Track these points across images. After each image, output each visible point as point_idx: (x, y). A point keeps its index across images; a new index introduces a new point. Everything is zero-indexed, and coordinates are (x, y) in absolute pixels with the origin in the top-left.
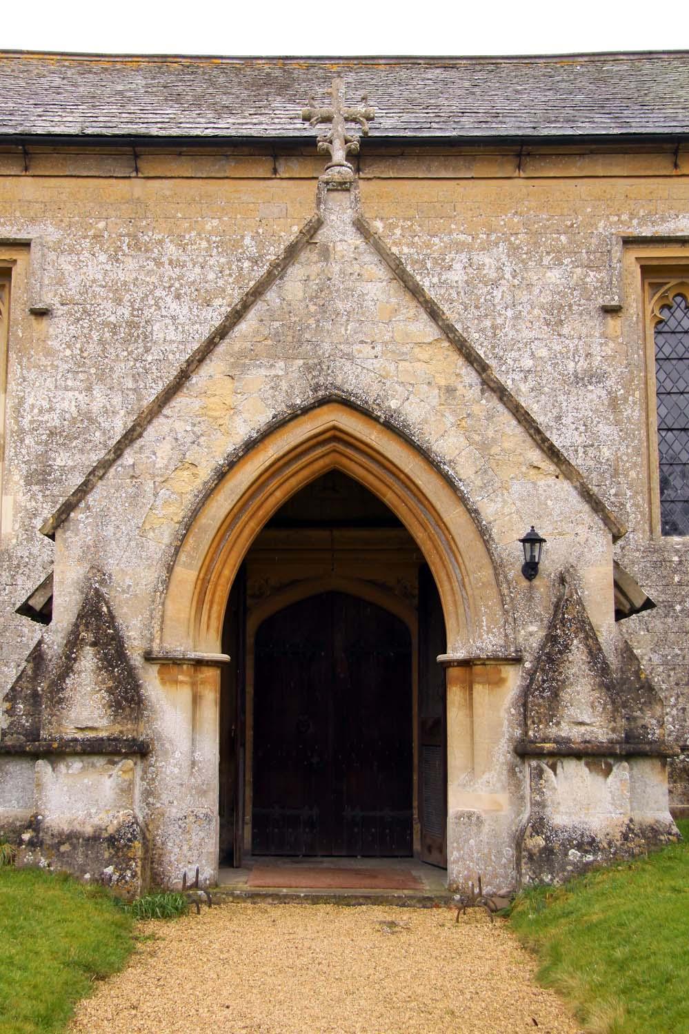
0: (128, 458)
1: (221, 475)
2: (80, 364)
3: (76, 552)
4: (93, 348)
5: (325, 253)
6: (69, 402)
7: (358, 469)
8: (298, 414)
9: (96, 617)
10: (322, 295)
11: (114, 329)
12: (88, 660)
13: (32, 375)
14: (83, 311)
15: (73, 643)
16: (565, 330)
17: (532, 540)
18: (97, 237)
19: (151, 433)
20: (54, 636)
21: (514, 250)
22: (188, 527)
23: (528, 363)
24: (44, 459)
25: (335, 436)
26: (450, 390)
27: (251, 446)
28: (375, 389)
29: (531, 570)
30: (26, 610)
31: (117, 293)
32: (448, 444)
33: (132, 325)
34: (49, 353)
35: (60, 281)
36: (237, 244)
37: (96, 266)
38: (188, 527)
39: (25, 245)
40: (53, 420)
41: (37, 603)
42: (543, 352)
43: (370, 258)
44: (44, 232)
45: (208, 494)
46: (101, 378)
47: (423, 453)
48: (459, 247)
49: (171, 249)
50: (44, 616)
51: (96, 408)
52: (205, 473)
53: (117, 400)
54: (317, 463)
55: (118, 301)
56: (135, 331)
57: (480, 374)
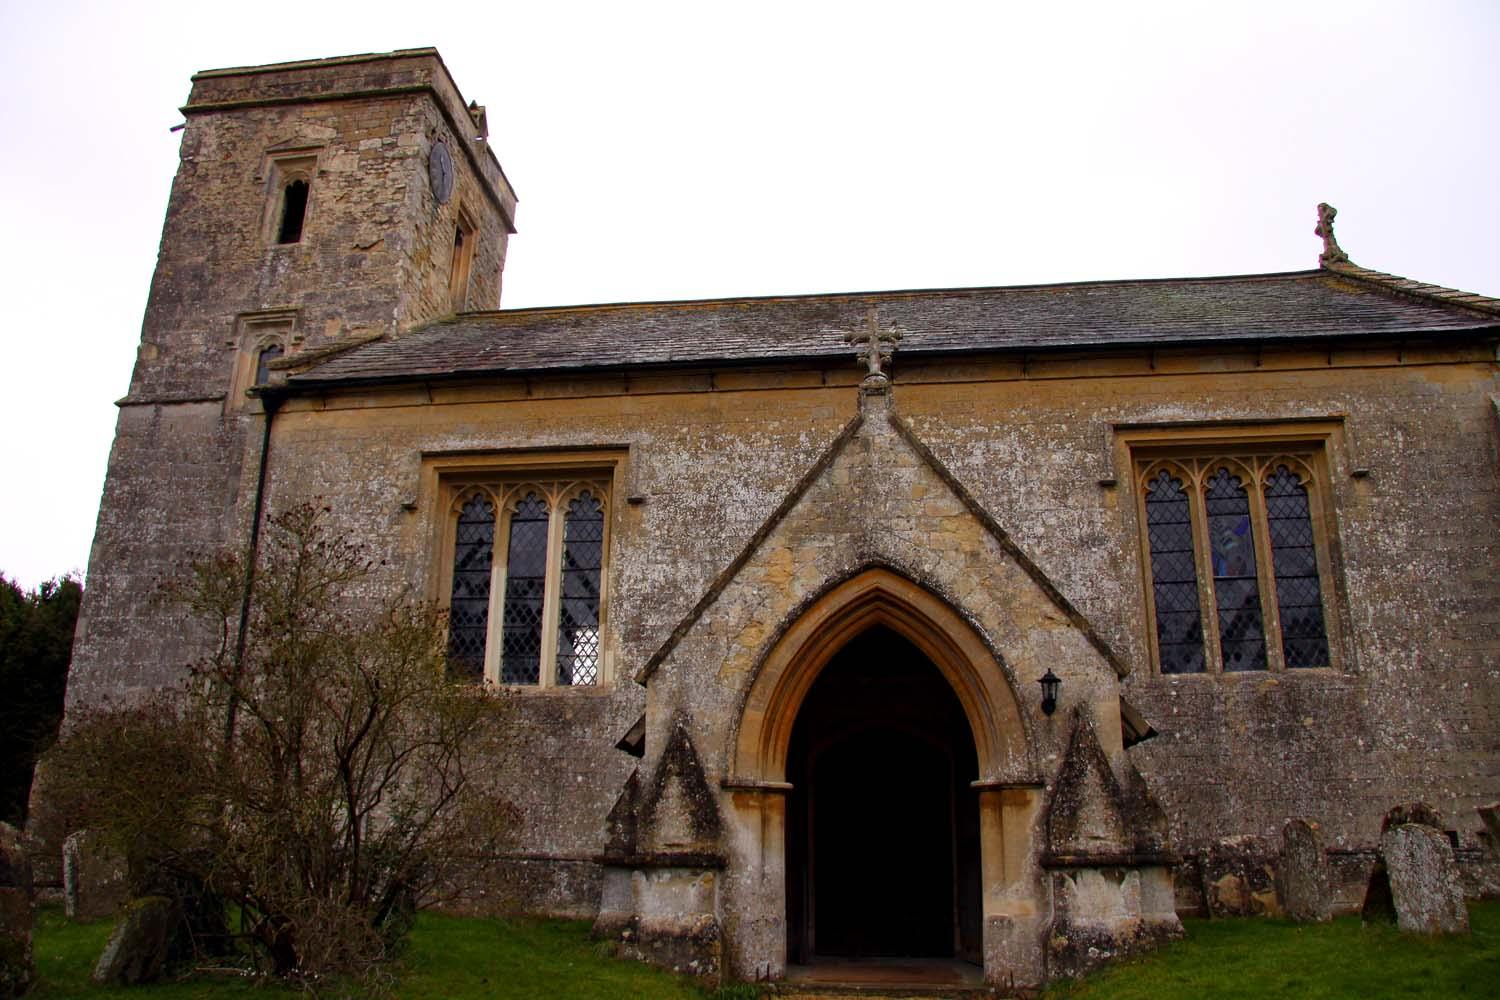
3: (664, 696)
4: (678, 529)
5: (866, 445)
6: (658, 574)
9: (681, 752)
11: (695, 512)
12: (674, 788)
13: (629, 551)
15: (662, 773)
16: (1071, 502)
17: (1050, 680)
19: (724, 597)
21: (1023, 438)
23: (1040, 530)
24: (638, 620)
26: (974, 555)
27: (807, 606)
29: (1049, 706)
30: (623, 745)
31: (697, 483)
32: (974, 600)
33: (709, 508)
34: (643, 533)
35: (652, 475)
36: (794, 440)
37: (680, 462)
42: (1053, 521)
46: (684, 552)
48: (979, 436)
49: (741, 447)
51: (680, 577)
52: (770, 628)
53: (697, 570)
54: (866, 617)
55: (698, 490)
56: (712, 515)
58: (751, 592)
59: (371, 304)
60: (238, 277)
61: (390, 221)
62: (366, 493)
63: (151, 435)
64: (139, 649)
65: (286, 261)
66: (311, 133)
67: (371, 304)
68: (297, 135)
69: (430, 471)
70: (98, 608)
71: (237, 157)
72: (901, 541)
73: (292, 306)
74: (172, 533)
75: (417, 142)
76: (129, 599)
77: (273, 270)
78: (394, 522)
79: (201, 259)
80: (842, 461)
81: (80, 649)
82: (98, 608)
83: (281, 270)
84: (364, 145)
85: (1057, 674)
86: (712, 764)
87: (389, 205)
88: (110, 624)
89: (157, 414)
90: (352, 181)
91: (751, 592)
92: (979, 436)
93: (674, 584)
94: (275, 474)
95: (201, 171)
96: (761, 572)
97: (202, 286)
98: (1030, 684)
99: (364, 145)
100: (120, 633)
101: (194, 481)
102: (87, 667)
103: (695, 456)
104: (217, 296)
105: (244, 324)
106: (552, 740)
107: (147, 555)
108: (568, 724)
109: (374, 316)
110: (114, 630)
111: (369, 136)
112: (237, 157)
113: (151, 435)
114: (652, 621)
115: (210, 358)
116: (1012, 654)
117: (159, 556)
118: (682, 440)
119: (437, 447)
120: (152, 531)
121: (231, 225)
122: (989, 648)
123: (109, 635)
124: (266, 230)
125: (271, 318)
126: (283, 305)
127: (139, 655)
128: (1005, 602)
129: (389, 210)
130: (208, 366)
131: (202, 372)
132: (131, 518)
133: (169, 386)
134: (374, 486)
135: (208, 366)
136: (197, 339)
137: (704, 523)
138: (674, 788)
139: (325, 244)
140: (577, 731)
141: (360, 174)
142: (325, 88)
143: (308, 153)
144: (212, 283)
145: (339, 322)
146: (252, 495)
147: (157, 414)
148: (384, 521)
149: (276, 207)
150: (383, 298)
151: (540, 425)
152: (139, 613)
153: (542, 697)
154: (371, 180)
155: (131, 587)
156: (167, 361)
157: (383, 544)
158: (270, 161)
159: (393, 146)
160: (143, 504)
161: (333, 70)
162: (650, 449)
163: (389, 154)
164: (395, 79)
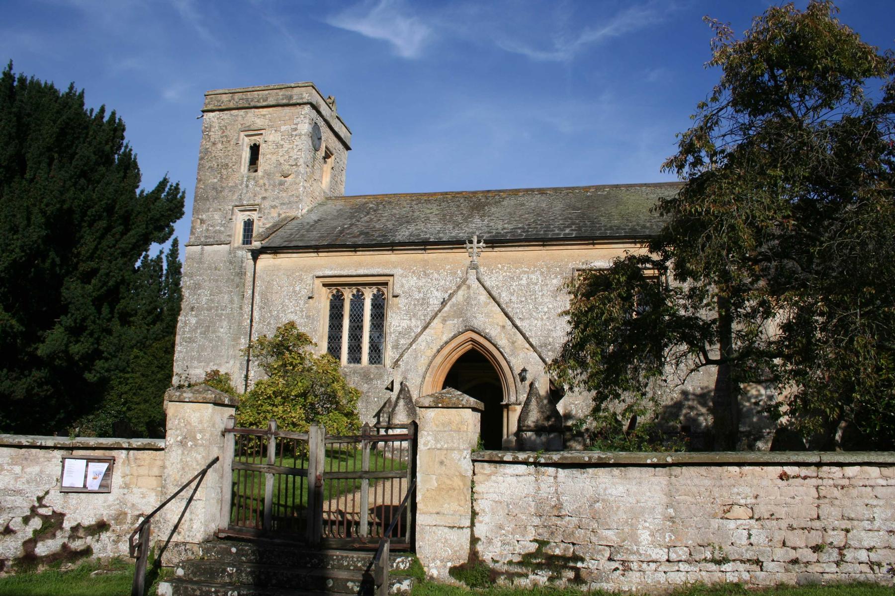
0: (414, 346)
1: (438, 351)
2: (408, 312)
3: (400, 373)
4: (412, 307)
5: (469, 287)
6: (405, 324)
7: (478, 348)
8: (460, 333)
9: (404, 389)
10: (468, 300)
11: (418, 300)
12: (401, 403)
13: (394, 315)
14: (409, 295)
15: (398, 398)
16: (558, 299)
17: (524, 370)
18: (414, 272)
19: (420, 339)
20: (394, 395)
21: (542, 273)
22: (429, 366)
23: (546, 310)
24: (397, 341)
25: (472, 340)
26: (503, 327)
27: (446, 343)
28: (482, 327)
29: (523, 379)
30: (387, 389)
31: (419, 290)
32: (502, 342)
33: (423, 299)
34: (399, 308)
35: (402, 286)
36: (456, 273)
37: (413, 281)
38: (429, 366)
39: (393, 275)
40: (400, 329)
41: (390, 387)
42: (551, 306)
43: (482, 289)
44: (398, 272)
45: (435, 356)
46: (414, 315)
47: (495, 346)
48: (525, 272)
49: (436, 275)
50: (392, 390)
51: (412, 325)
52: (435, 350)
53: (419, 323)
54: (469, 346)
55: (420, 292)
56: (424, 302)
57: (236, 456)
58: (429, 339)
59: (290, 203)
60: (233, 189)
61: (296, 165)
62: (294, 291)
63: (201, 259)
64: (202, 348)
65: (252, 182)
66: (259, 123)
67: (290, 203)
68: (254, 123)
69: (318, 282)
70: (184, 332)
71: (227, 133)
72: (479, 322)
73: (256, 202)
74: (212, 301)
75: (305, 128)
76: (197, 328)
77: (247, 186)
78: (306, 303)
79: (216, 180)
80: (460, 292)
81: (178, 348)
82: (184, 332)
83: (250, 186)
84: (283, 128)
85: (527, 368)
86: (415, 396)
87: (295, 157)
88: (190, 338)
89: (202, 250)
90: (279, 146)
91: (429, 339)
92: (525, 272)
93: (410, 328)
94: (258, 283)
95: (212, 140)
96: (432, 331)
97: (217, 193)
98: (517, 371)
99: (283, 128)
100: (194, 342)
101: (220, 278)
102: (182, 355)
103: (418, 279)
104: (224, 198)
105: (236, 209)
106: (366, 385)
107: (203, 310)
108: (372, 379)
109: (291, 208)
110: (191, 340)
111: (285, 124)
112: (227, 133)
113: (201, 259)
114: (402, 341)
115: (223, 225)
116: (513, 361)
117: (208, 310)
118: (414, 272)
119: (321, 274)
120: (204, 300)
121: (227, 165)
122: (505, 359)
123: (189, 342)
124: (242, 167)
125: (248, 208)
126: (252, 202)
127: (202, 351)
128: (513, 343)
129: (295, 160)
130: (222, 229)
131: (220, 231)
132: (195, 294)
133: (206, 237)
134: (297, 289)
135: (222, 229)
136: (216, 217)
137: (422, 305)
138: (401, 403)
139: (268, 174)
140: (375, 382)
141: (282, 143)
142: (264, 101)
143: (258, 132)
144: (221, 191)
145: (277, 210)
146: (250, 292)
147: (202, 250)
148: (302, 303)
149: (246, 154)
150: (295, 199)
151: (360, 265)
152: (201, 333)
153: (362, 368)
154: (287, 146)
155: (197, 323)
156: (204, 226)
157: (302, 311)
158: (242, 134)
159: (296, 129)
160: (199, 288)
161: (267, 92)
162: (401, 276)
163: (294, 133)
164: (295, 98)
